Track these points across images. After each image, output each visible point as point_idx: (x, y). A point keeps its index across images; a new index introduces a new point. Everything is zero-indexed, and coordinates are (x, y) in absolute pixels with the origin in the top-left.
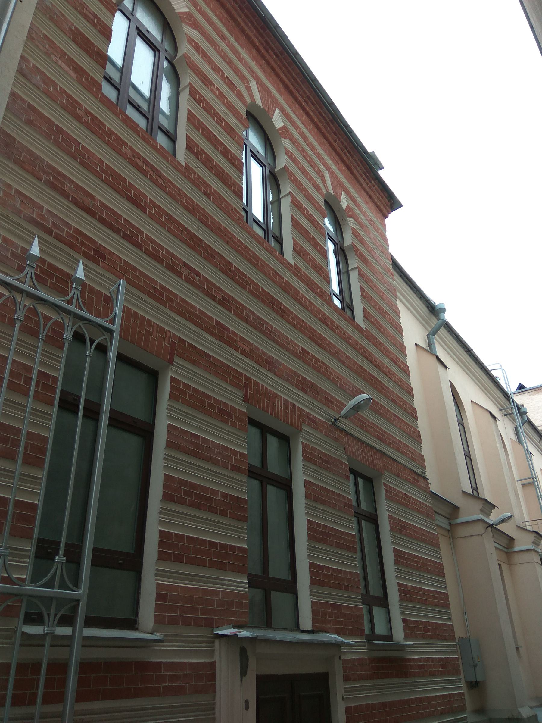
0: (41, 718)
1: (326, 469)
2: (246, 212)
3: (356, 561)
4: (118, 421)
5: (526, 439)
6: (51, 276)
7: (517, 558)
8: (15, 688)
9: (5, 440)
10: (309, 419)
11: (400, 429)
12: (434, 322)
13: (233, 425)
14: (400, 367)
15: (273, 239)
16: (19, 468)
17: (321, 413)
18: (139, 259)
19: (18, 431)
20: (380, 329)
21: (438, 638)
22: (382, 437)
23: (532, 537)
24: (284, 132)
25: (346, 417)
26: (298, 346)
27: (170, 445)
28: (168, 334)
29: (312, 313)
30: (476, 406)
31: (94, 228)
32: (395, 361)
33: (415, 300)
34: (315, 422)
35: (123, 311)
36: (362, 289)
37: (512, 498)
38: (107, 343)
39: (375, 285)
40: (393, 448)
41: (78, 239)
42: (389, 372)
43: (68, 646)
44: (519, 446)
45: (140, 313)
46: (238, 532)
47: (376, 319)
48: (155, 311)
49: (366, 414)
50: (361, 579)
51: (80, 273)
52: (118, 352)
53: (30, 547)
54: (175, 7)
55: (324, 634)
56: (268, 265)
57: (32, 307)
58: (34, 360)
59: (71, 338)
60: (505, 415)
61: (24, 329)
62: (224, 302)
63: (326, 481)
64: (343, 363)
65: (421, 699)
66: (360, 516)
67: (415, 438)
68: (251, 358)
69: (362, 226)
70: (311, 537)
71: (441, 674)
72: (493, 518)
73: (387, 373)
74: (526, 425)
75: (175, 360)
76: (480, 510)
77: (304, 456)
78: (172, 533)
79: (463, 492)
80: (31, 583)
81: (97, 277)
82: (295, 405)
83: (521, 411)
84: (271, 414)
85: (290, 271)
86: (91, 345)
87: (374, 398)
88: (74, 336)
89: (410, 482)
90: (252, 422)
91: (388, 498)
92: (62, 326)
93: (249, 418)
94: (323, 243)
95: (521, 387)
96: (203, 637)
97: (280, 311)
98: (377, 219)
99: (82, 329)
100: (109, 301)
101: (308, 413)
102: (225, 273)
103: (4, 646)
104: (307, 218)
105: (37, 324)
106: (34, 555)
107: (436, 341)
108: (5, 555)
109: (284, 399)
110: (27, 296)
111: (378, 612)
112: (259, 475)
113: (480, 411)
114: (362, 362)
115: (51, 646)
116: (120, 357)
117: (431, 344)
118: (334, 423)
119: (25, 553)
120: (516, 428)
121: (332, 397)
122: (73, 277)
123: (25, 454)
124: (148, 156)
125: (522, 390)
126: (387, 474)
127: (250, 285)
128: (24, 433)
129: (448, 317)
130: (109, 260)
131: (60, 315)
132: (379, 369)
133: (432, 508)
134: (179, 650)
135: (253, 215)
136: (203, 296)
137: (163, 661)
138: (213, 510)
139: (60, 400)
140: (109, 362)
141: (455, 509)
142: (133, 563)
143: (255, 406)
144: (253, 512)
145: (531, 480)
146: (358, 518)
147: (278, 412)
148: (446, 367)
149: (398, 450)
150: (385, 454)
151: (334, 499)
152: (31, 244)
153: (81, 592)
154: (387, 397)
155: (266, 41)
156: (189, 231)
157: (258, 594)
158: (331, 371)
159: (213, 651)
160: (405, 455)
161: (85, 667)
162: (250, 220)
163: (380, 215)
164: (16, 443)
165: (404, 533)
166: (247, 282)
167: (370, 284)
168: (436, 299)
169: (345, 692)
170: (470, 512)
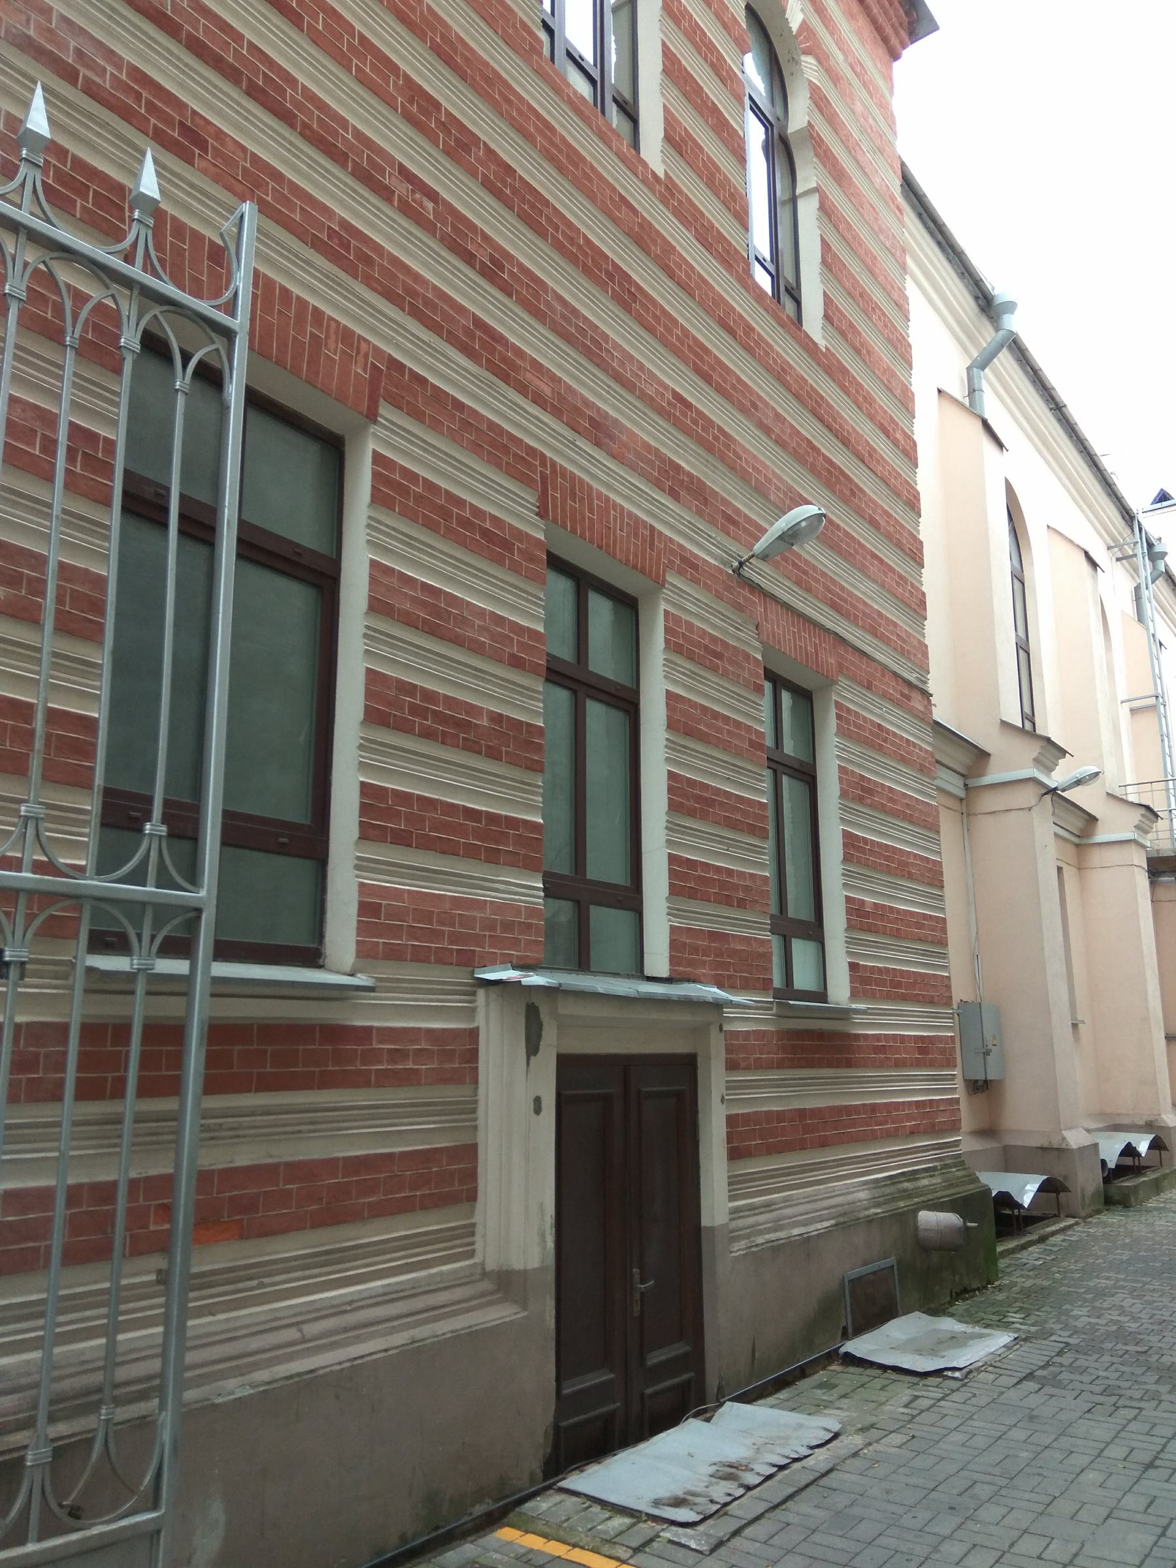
0: (136, 1122)
1: (714, 669)
2: (550, 32)
3: (764, 854)
4: (257, 549)
5: (1155, 613)
6: (82, 191)
7: (1097, 857)
8: (80, 1068)
9: (14, 580)
10: (684, 559)
11: (883, 586)
12: (988, 336)
13: (515, 568)
14: (896, 443)
15: (614, 108)
16: (47, 640)
17: (710, 548)
18: (289, 151)
19: (40, 561)
20: (860, 350)
21: (916, 1000)
22: (840, 604)
23: (1136, 816)
25: (764, 557)
26: (666, 387)
27: (377, 606)
28: (364, 346)
29: (702, 304)
30: (1058, 539)
31: (177, 67)
32: (887, 430)
33: (947, 278)
34: (695, 567)
35: (255, 284)
36: (825, 245)
37: (1106, 737)
38: (222, 364)
39: (856, 237)
40: (863, 628)
41: (138, 96)
42: (870, 455)
43: (184, 994)
45: (296, 290)
46: (525, 791)
47: (851, 325)
48: (331, 288)
49: (811, 551)
50: (772, 887)
51: (149, 184)
52: (247, 386)
53: (91, 804)
55: (692, 985)
56: (600, 176)
57: (42, 267)
58: (57, 397)
59: (137, 347)
60: (1118, 560)
61: (28, 322)
62: (496, 270)
63: (714, 695)
64: (767, 431)
65: (874, 1108)
66: (778, 766)
67: (914, 606)
68: (556, 412)
69: (835, 77)
70: (674, 807)
71: (918, 1064)
72: (1058, 777)
73: (867, 457)
75: (381, 411)
76: (1035, 760)
77: (667, 641)
78: (386, 789)
79: (1005, 724)
80: (98, 874)
81: (189, 194)
82: (652, 528)
84: (600, 547)
85: (654, 193)
86: (185, 367)
87: (830, 515)
88: (142, 342)
89: (891, 700)
90: (557, 564)
91: (841, 732)
92: (115, 317)
93: (549, 554)
94: (738, 123)
96: (452, 983)
97: (628, 296)
98: (873, 60)
99: (160, 325)
100: (219, 257)
101: (681, 546)
102: (497, 194)
103: (54, 991)
104: (700, 53)
105: (59, 310)
106: (98, 820)
108: (37, 819)
109: (630, 514)
110: (29, 239)
111: (802, 950)
112: (570, 677)
113: (1062, 547)
114: (810, 429)
115: (148, 993)
116: (254, 400)
117: (972, 391)
118: (737, 571)
119: (82, 817)
120: (1137, 589)
121: (737, 511)
122: (134, 194)
123: (58, 612)
126: (843, 681)
127: (557, 229)
128: (52, 566)
130: (217, 153)
131: (108, 288)
132: (848, 448)
133: (932, 754)
134: (405, 1005)
135: (566, 40)
136: (443, 253)
137: (376, 1024)
138: (471, 747)
139: (126, 494)
140: (229, 408)
141: (982, 756)
142: (309, 842)
143: (564, 526)
144: (558, 756)
145: (1153, 701)
146: (775, 771)
147: (615, 541)
148: (1000, 445)
149: (874, 632)
150: (843, 641)
151: (729, 731)
152: (26, 105)
153: (203, 893)
154: (860, 513)
156: (407, 77)
157: (564, 910)
158: (738, 449)
159: (474, 1010)
161: (220, 1033)
162: (560, 54)
163: (881, 51)
164: (38, 587)
165: (869, 801)
166: (549, 220)
167: (846, 233)
169: (728, 1088)
170: (1011, 762)
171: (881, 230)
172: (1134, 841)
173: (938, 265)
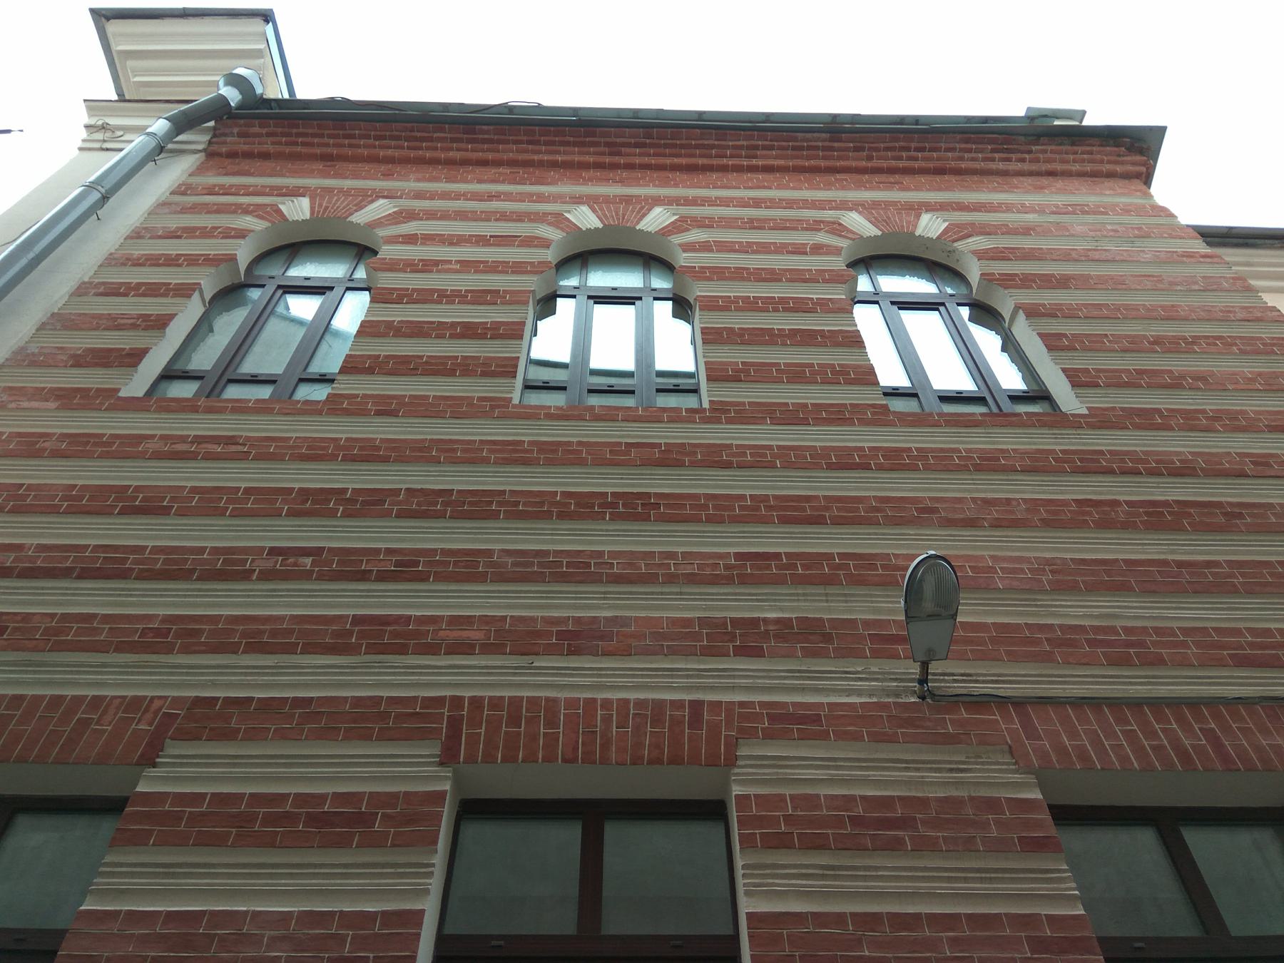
24: (958, 232)
54: (930, 235)
124: (1194, 446)
155: (607, 144)
171: (1171, 283)
173: (1267, 260)
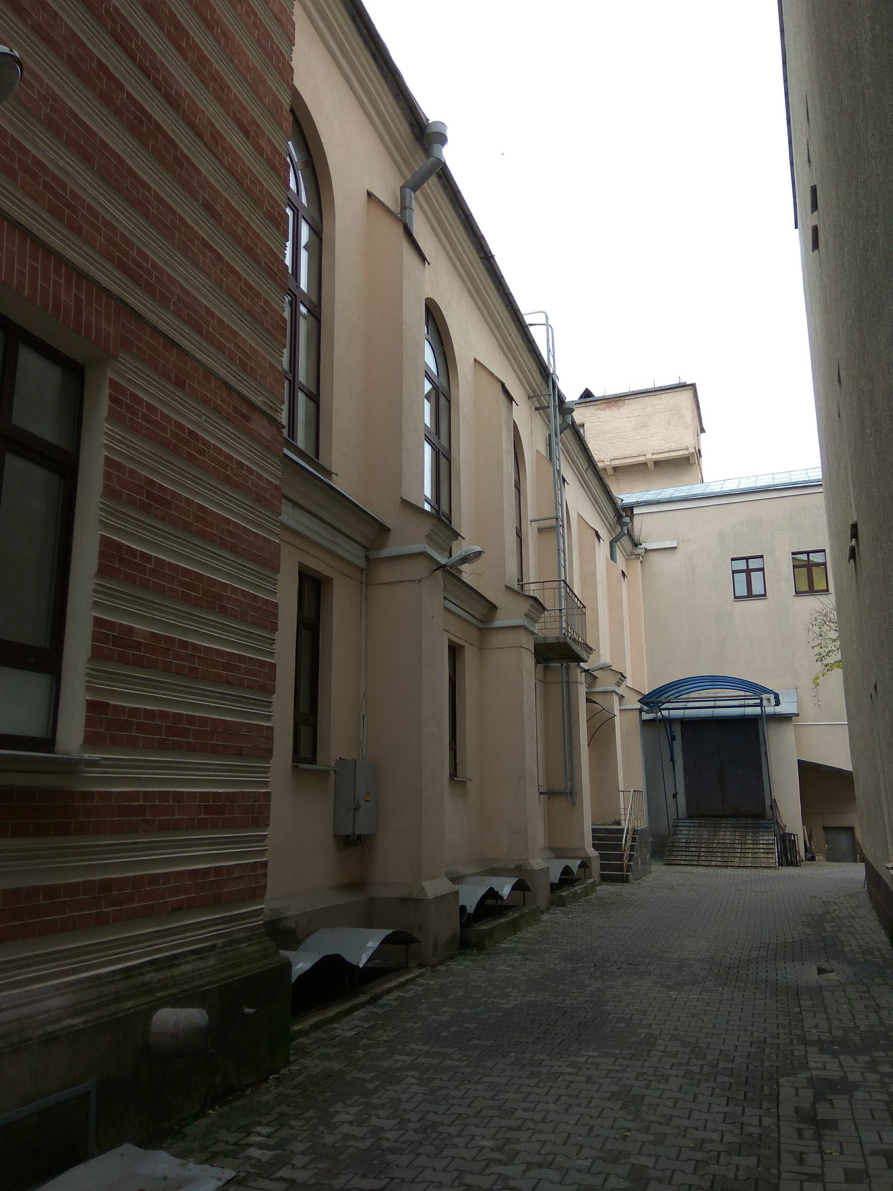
7: (496, 639)
12: (420, 162)
21: (214, 751)
22: (135, 269)
23: (525, 606)
44: (548, 466)
60: (536, 409)
71: (202, 826)
74: (568, 433)
76: (427, 536)
77: (110, 409)
83: (576, 431)
91: (114, 416)
95: (587, 394)
107: (415, 202)
113: (486, 380)
117: (404, 208)
125: (588, 399)
129: (450, 155)
133: (278, 488)
141: (383, 530)
145: (553, 523)
148: (423, 258)
149: (197, 327)
160: (221, 348)
168: (432, 110)
172: (424, 554)
